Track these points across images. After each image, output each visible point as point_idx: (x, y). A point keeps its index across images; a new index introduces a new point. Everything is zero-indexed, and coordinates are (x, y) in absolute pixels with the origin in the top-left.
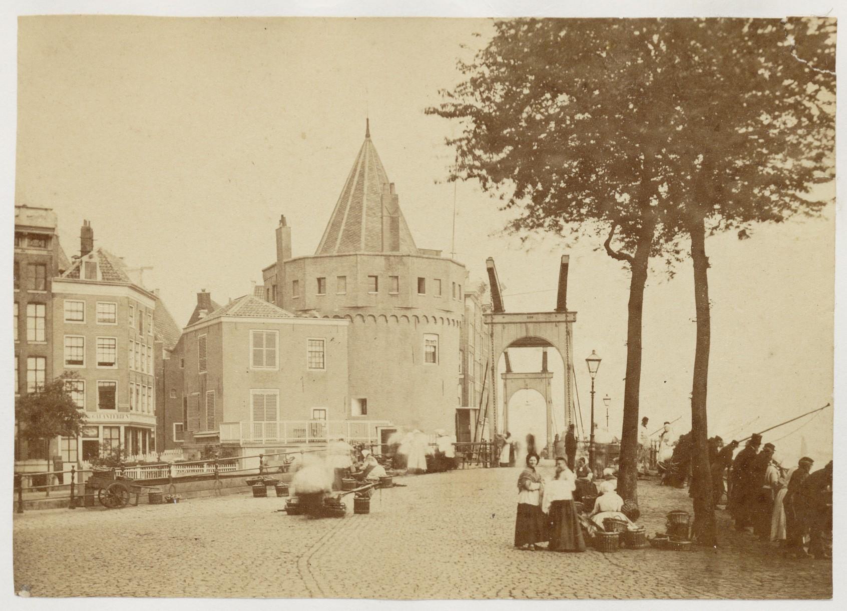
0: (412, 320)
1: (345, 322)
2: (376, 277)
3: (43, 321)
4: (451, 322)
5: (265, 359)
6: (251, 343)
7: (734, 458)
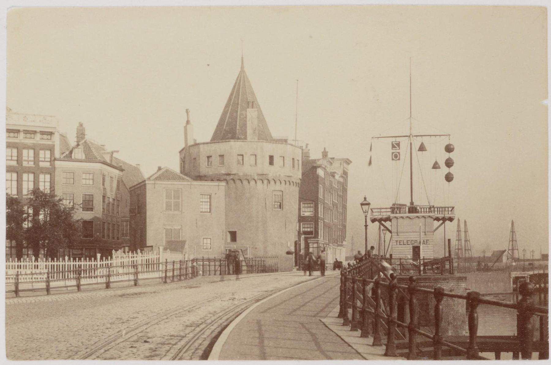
1: (224, 183)
3: (16, 182)
4: (292, 183)
5: (173, 208)
6: (165, 197)
7: (520, 353)
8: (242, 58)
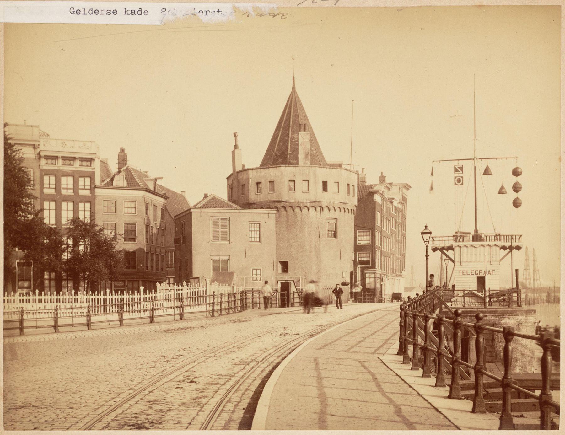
0: (319, 209)
2: (294, 181)
8: (294, 78)
